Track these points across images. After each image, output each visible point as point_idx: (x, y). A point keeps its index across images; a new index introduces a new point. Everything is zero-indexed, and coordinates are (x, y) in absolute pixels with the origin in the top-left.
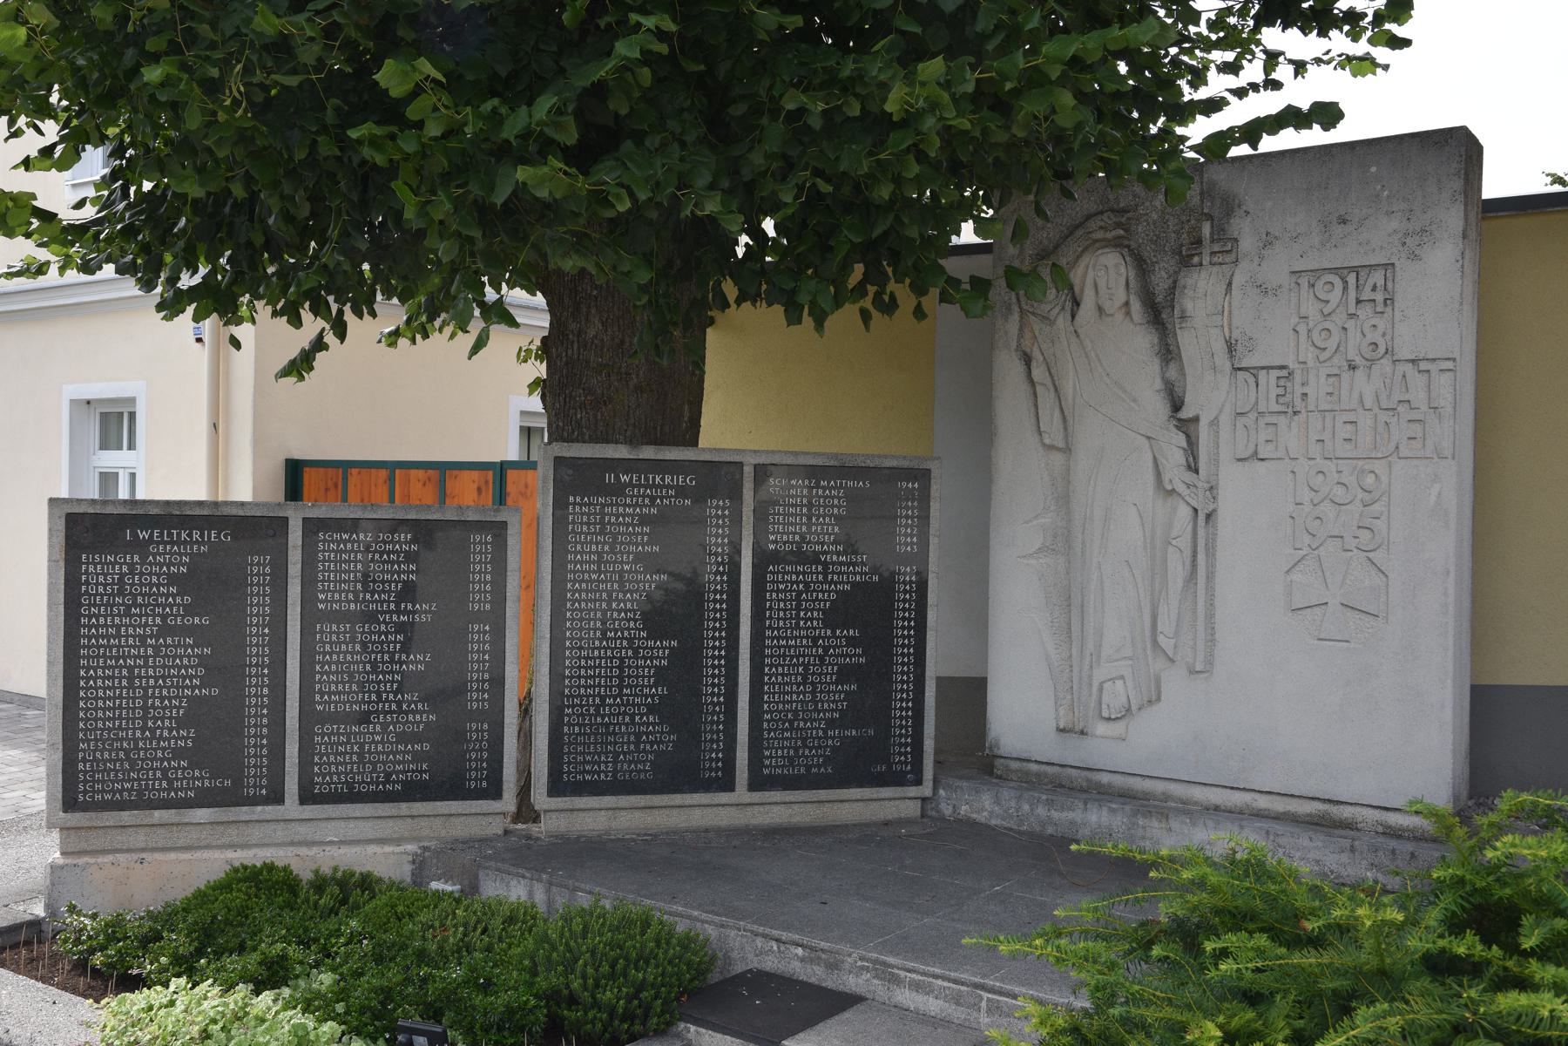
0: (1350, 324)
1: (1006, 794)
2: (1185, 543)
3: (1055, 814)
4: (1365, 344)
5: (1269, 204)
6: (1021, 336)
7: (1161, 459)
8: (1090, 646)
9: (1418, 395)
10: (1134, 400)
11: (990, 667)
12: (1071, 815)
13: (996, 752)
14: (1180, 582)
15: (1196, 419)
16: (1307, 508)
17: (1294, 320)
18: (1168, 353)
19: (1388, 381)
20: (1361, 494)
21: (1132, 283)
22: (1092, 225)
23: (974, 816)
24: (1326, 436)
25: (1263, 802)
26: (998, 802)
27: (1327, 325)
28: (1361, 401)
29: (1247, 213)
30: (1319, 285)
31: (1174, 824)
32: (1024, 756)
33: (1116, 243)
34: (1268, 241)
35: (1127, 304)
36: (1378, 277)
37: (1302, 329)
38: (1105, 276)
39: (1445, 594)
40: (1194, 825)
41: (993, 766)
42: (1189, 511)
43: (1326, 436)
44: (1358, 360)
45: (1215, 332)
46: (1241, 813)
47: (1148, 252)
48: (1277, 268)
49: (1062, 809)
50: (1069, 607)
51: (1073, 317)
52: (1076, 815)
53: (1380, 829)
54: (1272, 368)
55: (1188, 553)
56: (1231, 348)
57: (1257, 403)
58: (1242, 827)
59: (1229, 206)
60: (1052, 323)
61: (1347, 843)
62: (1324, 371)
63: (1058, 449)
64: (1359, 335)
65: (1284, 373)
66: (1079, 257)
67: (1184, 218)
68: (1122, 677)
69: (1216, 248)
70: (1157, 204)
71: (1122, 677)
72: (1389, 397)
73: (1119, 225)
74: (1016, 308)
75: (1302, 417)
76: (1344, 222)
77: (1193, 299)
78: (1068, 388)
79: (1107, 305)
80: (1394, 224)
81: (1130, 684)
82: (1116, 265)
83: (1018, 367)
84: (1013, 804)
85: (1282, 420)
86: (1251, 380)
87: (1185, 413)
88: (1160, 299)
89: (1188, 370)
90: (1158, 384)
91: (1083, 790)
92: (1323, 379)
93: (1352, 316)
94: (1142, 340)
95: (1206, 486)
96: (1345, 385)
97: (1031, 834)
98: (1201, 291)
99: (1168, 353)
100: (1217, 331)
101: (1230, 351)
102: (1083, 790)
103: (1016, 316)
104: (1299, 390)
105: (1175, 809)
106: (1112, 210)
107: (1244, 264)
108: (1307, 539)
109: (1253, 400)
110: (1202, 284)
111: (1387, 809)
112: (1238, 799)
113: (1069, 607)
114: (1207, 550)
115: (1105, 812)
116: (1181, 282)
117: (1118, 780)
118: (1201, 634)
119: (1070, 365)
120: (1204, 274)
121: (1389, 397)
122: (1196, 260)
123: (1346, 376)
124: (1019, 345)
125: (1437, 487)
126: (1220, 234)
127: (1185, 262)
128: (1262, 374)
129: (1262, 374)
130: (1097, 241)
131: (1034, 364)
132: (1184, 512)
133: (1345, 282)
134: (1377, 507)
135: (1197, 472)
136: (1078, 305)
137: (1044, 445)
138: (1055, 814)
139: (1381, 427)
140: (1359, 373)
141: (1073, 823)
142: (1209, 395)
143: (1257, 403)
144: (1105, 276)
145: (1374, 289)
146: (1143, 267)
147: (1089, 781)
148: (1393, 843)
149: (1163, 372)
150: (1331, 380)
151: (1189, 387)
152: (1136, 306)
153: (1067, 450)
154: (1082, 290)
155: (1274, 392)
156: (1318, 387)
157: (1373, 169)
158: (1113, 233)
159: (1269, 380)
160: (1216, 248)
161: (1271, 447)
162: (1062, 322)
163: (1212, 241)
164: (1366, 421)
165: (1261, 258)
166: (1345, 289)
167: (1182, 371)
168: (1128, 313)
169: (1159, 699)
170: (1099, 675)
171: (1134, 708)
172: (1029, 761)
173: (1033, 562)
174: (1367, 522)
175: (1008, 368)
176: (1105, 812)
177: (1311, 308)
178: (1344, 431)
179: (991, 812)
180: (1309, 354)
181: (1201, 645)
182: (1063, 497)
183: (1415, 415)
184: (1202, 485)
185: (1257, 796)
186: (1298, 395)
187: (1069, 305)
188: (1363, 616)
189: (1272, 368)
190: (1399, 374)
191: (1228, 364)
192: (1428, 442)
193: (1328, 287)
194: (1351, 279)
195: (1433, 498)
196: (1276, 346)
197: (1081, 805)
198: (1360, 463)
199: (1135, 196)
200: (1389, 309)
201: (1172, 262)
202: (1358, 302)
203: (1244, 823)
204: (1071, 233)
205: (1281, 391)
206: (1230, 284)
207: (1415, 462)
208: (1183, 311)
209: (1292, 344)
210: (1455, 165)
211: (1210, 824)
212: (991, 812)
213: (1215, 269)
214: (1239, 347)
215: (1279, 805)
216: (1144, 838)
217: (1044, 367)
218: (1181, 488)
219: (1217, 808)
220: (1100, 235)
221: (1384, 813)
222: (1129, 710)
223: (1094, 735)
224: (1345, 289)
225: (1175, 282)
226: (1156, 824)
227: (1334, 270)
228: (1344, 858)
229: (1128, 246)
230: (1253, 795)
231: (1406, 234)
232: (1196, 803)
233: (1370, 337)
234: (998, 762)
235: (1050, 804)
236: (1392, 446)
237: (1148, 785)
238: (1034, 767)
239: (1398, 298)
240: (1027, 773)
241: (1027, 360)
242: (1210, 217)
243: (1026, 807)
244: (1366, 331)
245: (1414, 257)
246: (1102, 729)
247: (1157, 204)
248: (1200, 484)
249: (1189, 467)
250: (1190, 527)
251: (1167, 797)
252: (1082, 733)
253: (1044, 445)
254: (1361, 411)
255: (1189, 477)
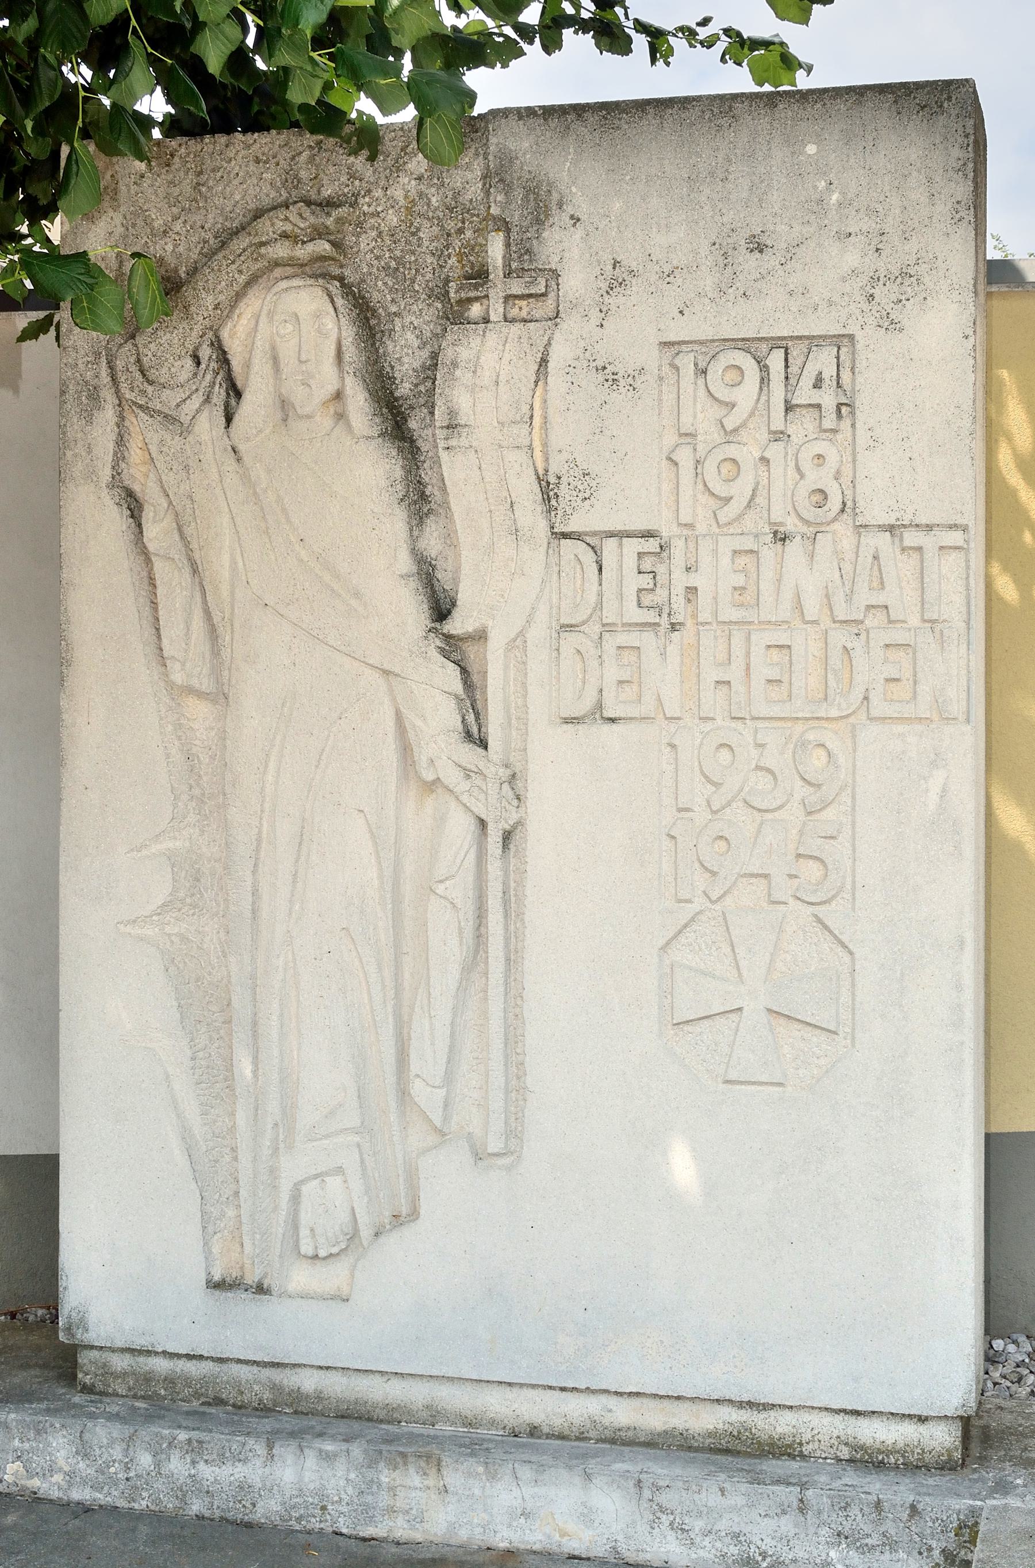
0: (775, 451)
1: (101, 1432)
2: (460, 890)
3: (207, 1472)
4: (803, 491)
5: (617, 205)
6: (120, 456)
7: (408, 714)
8: (273, 1107)
9: (900, 595)
10: (357, 595)
11: (62, 1139)
12: (239, 1472)
13: (80, 1336)
14: (454, 972)
15: (481, 636)
16: (701, 815)
17: (670, 439)
18: (420, 500)
19: (847, 567)
20: (801, 791)
21: (351, 353)
22: (266, 228)
23: (35, 1483)
24: (735, 673)
25: (624, 1415)
26: (84, 1451)
27: (732, 451)
28: (799, 606)
29: (576, 220)
30: (716, 371)
31: (453, 1477)
32: (139, 1342)
33: (317, 270)
34: (617, 279)
35: (338, 396)
36: (823, 361)
37: (685, 457)
38: (290, 332)
39: (959, 987)
40: (492, 1477)
41: (75, 1364)
42: (472, 826)
43: (735, 673)
44: (791, 524)
45: (516, 459)
46: (581, 1438)
47: (379, 292)
48: (634, 332)
49: (222, 1459)
50: (216, 1016)
51: (229, 419)
52: (251, 1471)
53: (845, 1453)
54: (629, 535)
55: (469, 908)
56: (548, 491)
57: (599, 605)
58: (588, 1477)
59: (541, 205)
60: (185, 430)
61: (789, 1494)
62: (727, 544)
63: (200, 694)
64: (791, 472)
65: (652, 545)
66: (239, 296)
67: (451, 225)
68: (339, 1170)
69: (517, 287)
70: (398, 194)
71: (339, 1170)
72: (849, 597)
73: (319, 233)
74: (108, 395)
75: (688, 633)
76: (760, 248)
77: (472, 389)
78: (220, 564)
79: (298, 395)
80: (852, 258)
81: (356, 1185)
82: (317, 316)
83: (114, 519)
84: (117, 1452)
85: (648, 640)
86: (588, 558)
87: (455, 625)
88: (404, 389)
89: (464, 537)
90: (405, 563)
91: (264, 1410)
92: (725, 561)
93: (779, 436)
94: (370, 469)
95: (504, 773)
96: (768, 574)
97: (156, 1517)
98: (486, 376)
99: (420, 500)
100: (522, 456)
101: (547, 499)
102: (264, 1410)
103: (108, 415)
104: (680, 580)
105: (453, 1439)
106: (309, 203)
107: (571, 324)
108: (701, 880)
109: (593, 598)
110: (488, 360)
111: (857, 1413)
112: (577, 1410)
113: (216, 1016)
114: (506, 903)
115: (311, 1461)
116: (448, 354)
117: (336, 1386)
118: (498, 1079)
119: (226, 520)
120: (492, 339)
121: (849, 597)
122: (476, 310)
123: (769, 553)
124: (117, 473)
125: (938, 778)
126: (522, 258)
127: (454, 315)
128: (610, 546)
129: (610, 546)
130: (277, 264)
131: (148, 516)
132: (459, 828)
133: (764, 369)
134: (829, 814)
135: (483, 744)
136: (239, 395)
137: (171, 685)
138: (207, 1472)
139: (836, 659)
140: (794, 547)
141: (243, 1487)
142: (503, 587)
143: (599, 605)
144: (290, 332)
145: (818, 384)
146: (368, 321)
147: (276, 1388)
148: (875, 1485)
149: (413, 539)
150: (742, 561)
151: (466, 570)
152: (358, 401)
153: (220, 696)
154: (247, 365)
155: (634, 582)
156: (716, 575)
157: (811, 149)
158: (310, 247)
159: (622, 557)
160: (517, 287)
161: (630, 692)
162: (208, 425)
163: (507, 275)
164: (806, 645)
165: (605, 312)
166: (764, 381)
167: (450, 538)
168: (341, 416)
169: (414, 1214)
170: (292, 1168)
171: (366, 1233)
172: (149, 1353)
173: (150, 931)
174: (814, 845)
175: (92, 521)
176: (311, 1461)
177: (702, 418)
178: (764, 668)
179: (70, 1475)
180: (696, 508)
181: (497, 1102)
182: (206, 786)
183: (899, 636)
184: (495, 771)
185: (612, 1402)
186: (678, 589)
187: (219, 395)
188: (807, 1033)
189: (629, 535)
190: (866, 558)
191: (542, 525)
192: (923, 688)
193: (732, 376)
194: (776, 361)
195: (933, 797)
196: (628, 495)
197: (261, 1449)
198: (799, 727)
199: (352, 176)
200: (846, 424)
201: (430, 314)
202: (789, 408)
203: (592, 1464)
204: (223, 244)
205: (740, 580)
206: (544, 362)
207: (900, 728)
208: (452, 413)
209: (666, 487)
210: (956, 152)
211: (526, 1473)
212: (70, 1475)
213: (516, 329)
214: (563, 490)
215: (654, 1419)
216: (391, 1511)
217: (168, 522)
218: (452, 777)
219: (534, 1431)
220: (281, 250)
221: (852, 1420)
222: (354, 1236)
223: (285, 1295)
224: (764, 381)
225: (435, 356)
226: (416, 1480)
227: (743, 344)
228: (787, 1525)
229: (341, 279)
230: (603, 1399)
231: (875, 279)
232: (493, 1423)
233: (816, 477)
234: (84, 1358)
235: (195, 1449)
236: (858, 694)
237: (395, 1392)
238: (161, 1365)
239: (862, 402)
240: (148, 1378)
241: (133, 506)
242: (504, 225)
243: (145, 1460)
244: (806, 466)
245: (891, 325)
246: (301, 1277)
247: (398, 194)
248: (490, 771)
249: (468, 735)
250: (472, 856)
251: (434, 1415)
252: (261, 1289)
253: (171, 685)
254: (797, 623)
255: (469, 754)
